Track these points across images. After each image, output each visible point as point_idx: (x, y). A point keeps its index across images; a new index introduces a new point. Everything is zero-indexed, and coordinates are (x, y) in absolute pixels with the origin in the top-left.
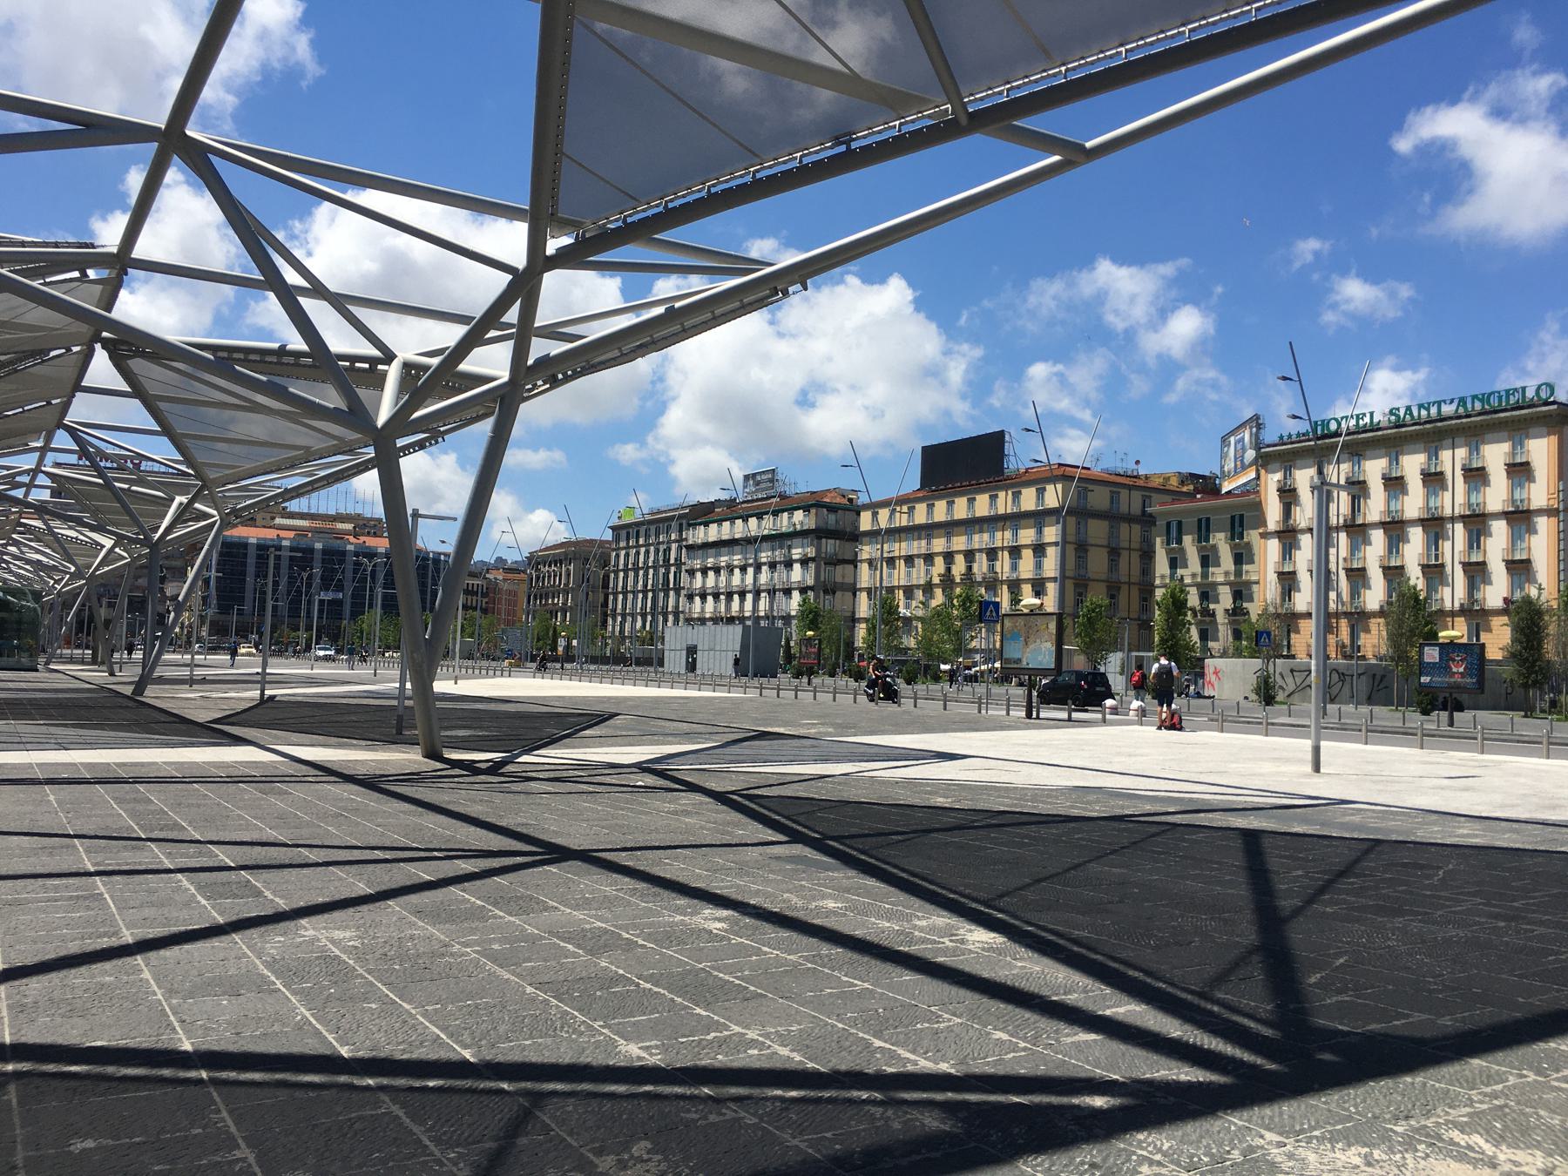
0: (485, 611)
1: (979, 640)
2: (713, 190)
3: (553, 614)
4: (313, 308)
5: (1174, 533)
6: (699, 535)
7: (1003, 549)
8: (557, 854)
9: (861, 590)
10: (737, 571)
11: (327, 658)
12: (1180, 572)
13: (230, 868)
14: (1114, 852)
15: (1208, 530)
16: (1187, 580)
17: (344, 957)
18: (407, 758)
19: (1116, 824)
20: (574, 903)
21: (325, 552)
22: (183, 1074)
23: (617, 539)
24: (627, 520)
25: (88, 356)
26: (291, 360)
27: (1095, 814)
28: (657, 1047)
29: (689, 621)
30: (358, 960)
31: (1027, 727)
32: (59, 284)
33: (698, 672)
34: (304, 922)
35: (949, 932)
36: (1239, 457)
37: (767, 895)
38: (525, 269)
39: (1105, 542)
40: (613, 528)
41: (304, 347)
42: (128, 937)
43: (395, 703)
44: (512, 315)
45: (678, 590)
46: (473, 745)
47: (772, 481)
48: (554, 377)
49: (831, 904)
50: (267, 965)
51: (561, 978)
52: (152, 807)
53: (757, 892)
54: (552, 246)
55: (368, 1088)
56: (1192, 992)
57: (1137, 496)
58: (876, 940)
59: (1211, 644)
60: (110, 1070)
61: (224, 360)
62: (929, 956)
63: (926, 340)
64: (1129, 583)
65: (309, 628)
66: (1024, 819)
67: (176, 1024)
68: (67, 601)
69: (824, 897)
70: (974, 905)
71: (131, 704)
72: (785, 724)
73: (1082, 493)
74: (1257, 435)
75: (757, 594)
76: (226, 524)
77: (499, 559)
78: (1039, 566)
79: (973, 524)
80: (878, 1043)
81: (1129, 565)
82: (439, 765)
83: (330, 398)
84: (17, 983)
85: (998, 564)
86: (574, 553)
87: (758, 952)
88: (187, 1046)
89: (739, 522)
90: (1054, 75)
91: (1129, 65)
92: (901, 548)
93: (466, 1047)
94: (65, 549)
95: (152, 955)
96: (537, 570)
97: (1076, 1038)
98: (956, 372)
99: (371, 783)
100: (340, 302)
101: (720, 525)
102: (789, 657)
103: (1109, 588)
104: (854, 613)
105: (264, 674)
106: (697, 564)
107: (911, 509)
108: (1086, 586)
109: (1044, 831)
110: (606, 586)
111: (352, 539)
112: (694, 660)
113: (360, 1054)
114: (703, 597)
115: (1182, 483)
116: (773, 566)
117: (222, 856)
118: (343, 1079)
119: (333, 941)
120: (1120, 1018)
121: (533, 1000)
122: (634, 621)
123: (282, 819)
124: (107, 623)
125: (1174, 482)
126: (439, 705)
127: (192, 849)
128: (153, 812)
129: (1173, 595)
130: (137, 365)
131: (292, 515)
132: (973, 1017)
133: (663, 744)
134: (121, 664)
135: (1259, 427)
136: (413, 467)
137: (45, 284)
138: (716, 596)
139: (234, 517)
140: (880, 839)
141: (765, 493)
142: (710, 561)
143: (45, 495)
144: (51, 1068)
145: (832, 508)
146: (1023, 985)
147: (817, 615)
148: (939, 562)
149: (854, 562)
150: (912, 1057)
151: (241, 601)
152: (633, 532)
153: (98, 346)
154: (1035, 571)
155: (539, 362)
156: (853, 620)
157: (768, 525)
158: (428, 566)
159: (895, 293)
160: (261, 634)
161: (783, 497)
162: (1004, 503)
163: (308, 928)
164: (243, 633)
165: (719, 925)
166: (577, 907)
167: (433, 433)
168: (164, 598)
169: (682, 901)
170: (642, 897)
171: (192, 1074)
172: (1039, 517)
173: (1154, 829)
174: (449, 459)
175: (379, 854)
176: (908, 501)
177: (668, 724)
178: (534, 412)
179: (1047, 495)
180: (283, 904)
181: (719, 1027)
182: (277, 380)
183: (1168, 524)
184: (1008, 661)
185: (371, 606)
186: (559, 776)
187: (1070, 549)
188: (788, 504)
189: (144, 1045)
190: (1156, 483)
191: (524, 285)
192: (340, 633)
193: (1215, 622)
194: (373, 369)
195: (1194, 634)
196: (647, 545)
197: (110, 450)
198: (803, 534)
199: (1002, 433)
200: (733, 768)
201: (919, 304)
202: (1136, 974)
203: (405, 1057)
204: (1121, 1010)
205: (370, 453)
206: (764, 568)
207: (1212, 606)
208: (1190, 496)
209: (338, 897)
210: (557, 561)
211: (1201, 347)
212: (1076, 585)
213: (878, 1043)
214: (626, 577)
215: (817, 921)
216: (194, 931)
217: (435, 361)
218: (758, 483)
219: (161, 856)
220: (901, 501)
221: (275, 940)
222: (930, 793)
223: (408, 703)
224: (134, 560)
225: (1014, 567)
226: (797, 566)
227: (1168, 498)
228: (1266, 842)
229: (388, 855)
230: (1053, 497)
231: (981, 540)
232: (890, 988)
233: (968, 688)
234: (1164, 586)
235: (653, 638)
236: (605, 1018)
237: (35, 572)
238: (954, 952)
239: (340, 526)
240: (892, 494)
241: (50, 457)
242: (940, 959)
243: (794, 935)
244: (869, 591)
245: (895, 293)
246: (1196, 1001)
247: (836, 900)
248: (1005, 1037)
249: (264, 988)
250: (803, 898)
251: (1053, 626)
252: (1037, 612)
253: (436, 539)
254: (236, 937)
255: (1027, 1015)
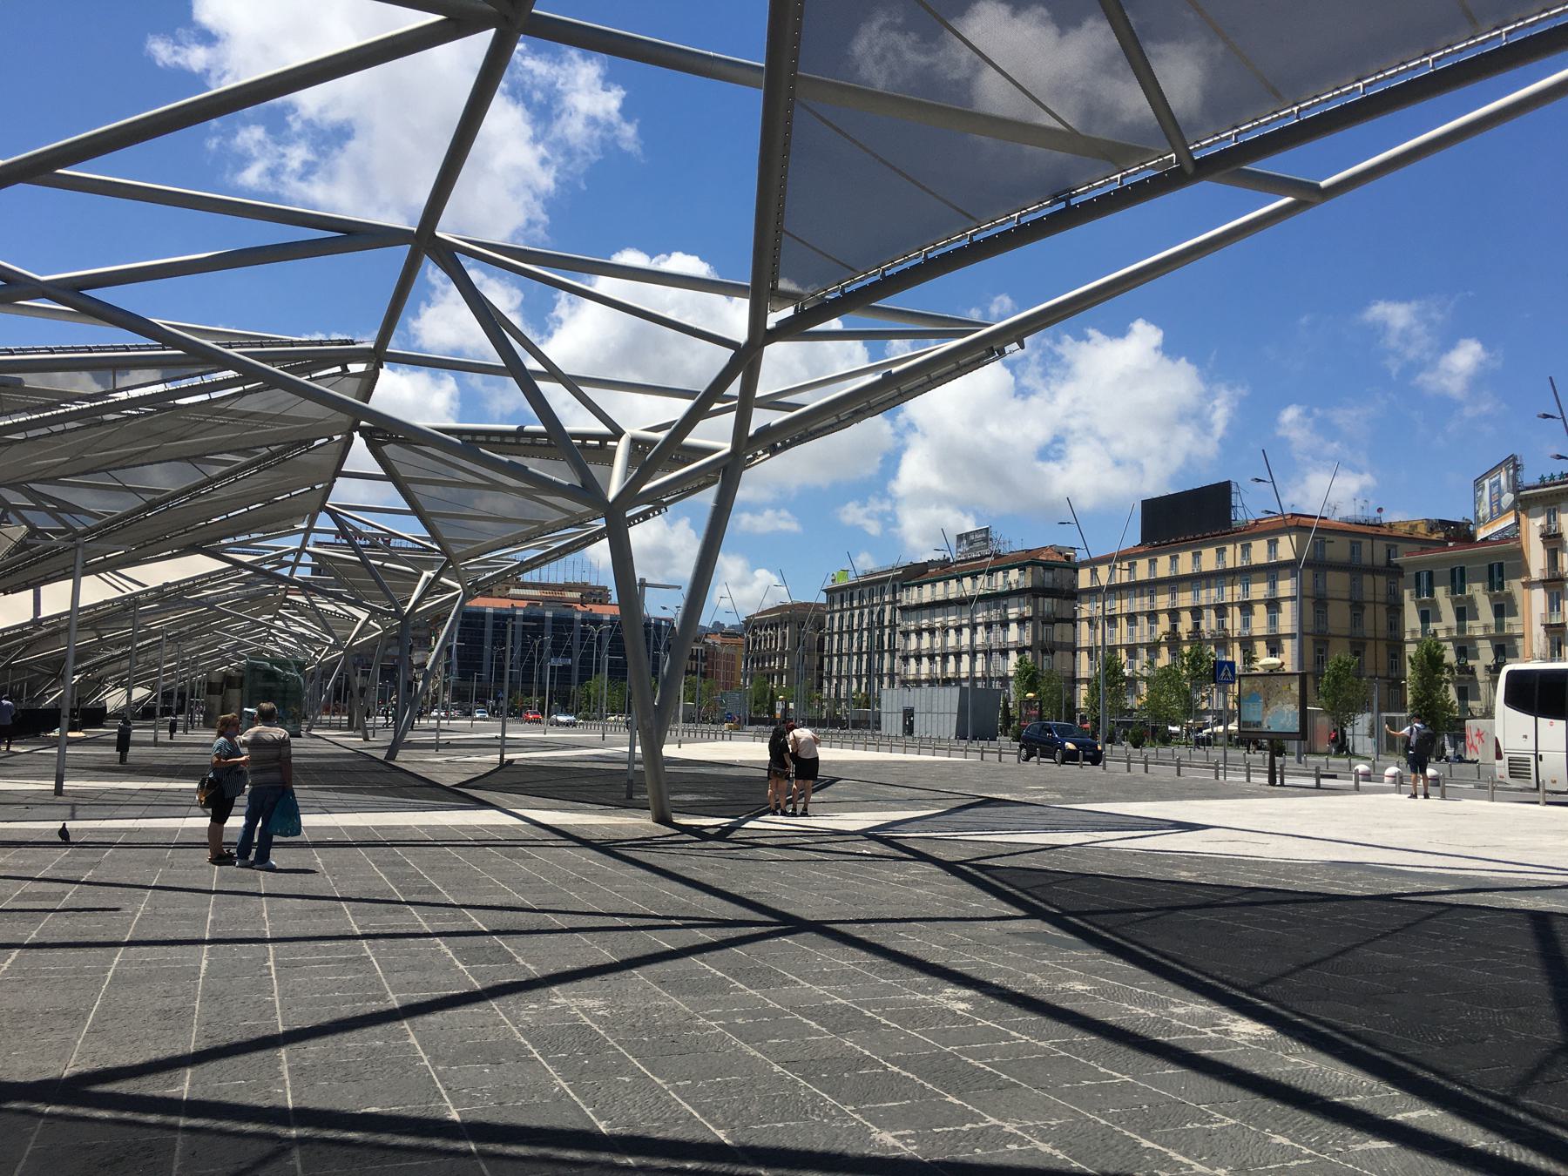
0: (704, 675)
1: (1212, 699)
2: (930, 256)
3: (770, 677)
4: (553, 392)
5: (1424, 585)
6: (913, 596)
7: (1232, 604)
8: (791, 925)
9: (1081, 649)
10: (952, 632)
11: (567, 724)
12: (1432, 626)
13: (483, 933)
14: (1384, 935)
15: (1463, 581)
16: (1442, 635)
17: (595, 1027)
18: (636, 823)
19: (1384, 905)
20: (816, 977)
21: (554, 620)
22: (453, 1145)
23: (831, 601)
24: (842, 582)
25: (348, 442)
26: (528, 441)
27: (1358, 893)
28: (911, 1136)
29: (904, 683)
30: (608, 1030)
31: (1271, 795)
32: (323, 379)
33: (883, 732)
34: (555, 989)
35: (1210, 1021)
36: (1495, 501)
37: (1009, 974)
38: (748, 343)
39: (1346, 596)
40: (826, 591)
41: (542, 428)
42: (394, 1002)
43: (624, 767)
44: (734, 389)
45: (893, 652)
46: (701, 810)
47: (985, 540)
48: (774, 445)
49: (1079, 987)
50: (524, 1033)
51: (807, 1057)
52: (409, 871)
53: (1000, 970)
54: (772, 320)
55: (628, 1168)
56: (1492, 1097)
57: (1380, 547)
58: (1131, 1028)
59: (1471, 704)
60: (384, 1138)
61: (470, 444)
62: (1192, 1048)
63: (1180, 381)
64: (1376, 639)
65: (541, 693)
66: (1279, 897)
67: (443, 1092)
68: (326, 670)
69: (1070, 978)
70: (1234, 992)
71: (384, 768)
72: (1010, 790)
73: (1319, 545)
74: (1514, 477)
75: (973, 654)
76: (468, 596)
77: (717, 624)
78: (1273, 622)
79: (1199, 580)
80: (1146, 1143)
81: (1376, 619)
82: (669, 830)
83: (561, 473)
84: (296, 1046)
85: (1228, 621)
86: (790, 617)
87: (1008, 1037)
88: (454, 1116)
89: (953, 582)
90: (1286, 116)
91: (1368, 100)
92: (1122, 606)
93: (719, 1127)
94: (324, 621)
95: (418, 1020)
96: (754, 634)
97: (1366, 1146)
98: (1220, 415)
99: (607, 847)
100: (572, 384)
101: (934, 586)
102: (1008, 719)
103: (1352, 644)
104: (1074, 673)
105: (503, 738)
106: (912, 625)
107: (1132, 566)
108: (1327, 643)
109: (1302, 910)
110: (821, 649)
111: (579, 607)
112: (912, 723)
113: (618, 1130)
114: (918, 659)
115: (1432, 530)
116: (988, 626)
117: (475, 921)
118: (604, 1157)
119: (583, 1010)
120: (1414, 1124)
121: (781, 1079)
122: (850, 683)
123: (527, 883)
124: (362, 690)
125: (1422, 530)
126: (668, 769)
127: (447, 912)
128: (410, 875)
129: (1428, 652)
130: (390, 450)
131: (525, 586)
132: (1248, 1119)
133: (888, 810)
134: (374, 729)
135: (1516, 468)
136: (639, 535)
137: (311, 379)
138: (931, 658)
139: (484, 589)
140: (1123, 915)
141: (978, 553)
142: (925, 623)
143: (303, 573)
144: (330, 1134)
145: (1049, 566)
146: (1297, 1082)
147: (1035, 674)
148: (1164, 620)
149: (1073, 621)
150: (1186, 1161)
151: (479, 668)
152: (847, 595)
153: (356, 435)
154: (1270, 629)
155: (760, 432)
156: (1074, 681)
157: (982, 585)
158: (655, 631)
159: (1144, 338)
160: (498, 700)
161: (998, 556)
162: (1233, 557)
163: (559, 996)
164: (482, 699)
165: (963, 1006)
166: (816, 982)
167: (657, 502)
168: (412, 667)
169: (922, 979)
170: (880, 973)
171: (461, 1145)
172: (1272, 571)
173: (1427, 910)
174: (683, 525)
175: (620, 921)
176: (1129, 556)
177: (885, 788)
178: (766, 476)
179: (1279, 547)
180: (534, 971)
181: (975, 1118)
182: (516, 459)
183: (1418, 575)
184: (1247, 724)
185: (597, 671)
186: (785, 844)
187: (1308, 604)
188: (1003, 563)
189: (414, 1114)
190: (1402, 531)
191: (746, 359)
192: (566, 696)
193: (1475, 681)
194: (602, 445)
195: (1452, 694)
196: (861, 607)
197: (365, 530)
198: (1019, 593)
199: (1227, 484)
200: (961, 836)
201: (1170, 349)
202: (1427, 1075)
203: (661, 1135)
204: (1414, 1115)
205: (601, 524)
206: (980, 629)
207: (1470, 663)
208: (1442, 544)
209: (585, 965)
210: (773, 625)
211: (1479, 381)
212: (1315, 642)
213: (1146, 1143)
214: (841, 639)
215: (1066, 1005)
216: (454, 996)
217: (662, 435)
218: (971, 543)
219: (419, 920)
220: (1122, 557)
221: (529, 1007)
222: (1172, 866)
223: (638, 767)
224: (386, 631)
225: (1246, 624)
226: (1013, 626)
227: (1417, 547)
228: (1558, 925)
229: (628, 922)
230: (1286, 549)
231: (1208, 596)
232: (1152, 1081)
233: (1200, 752)
234: (1416, 641)
235: (871, 700)
236: (856, 1102)
237: (299, 645)
238: (1218, 1044)
239: (569, 595)
240: (1113, 549)
241: (313, 537)
242: (1204, 1052)
243: (1043, 1020)
244: (1090, 650)
245: (1144, 338)
246: (1499, 1106)
247: (1083, 981)
248: (1286, 1142)
249: (521, 1056)
250: (1048, 978)
251: (1295, 687)
252: (1274, 673)
253: (662, 606)
254: (493, 1003)
255: (1308, 1118)
